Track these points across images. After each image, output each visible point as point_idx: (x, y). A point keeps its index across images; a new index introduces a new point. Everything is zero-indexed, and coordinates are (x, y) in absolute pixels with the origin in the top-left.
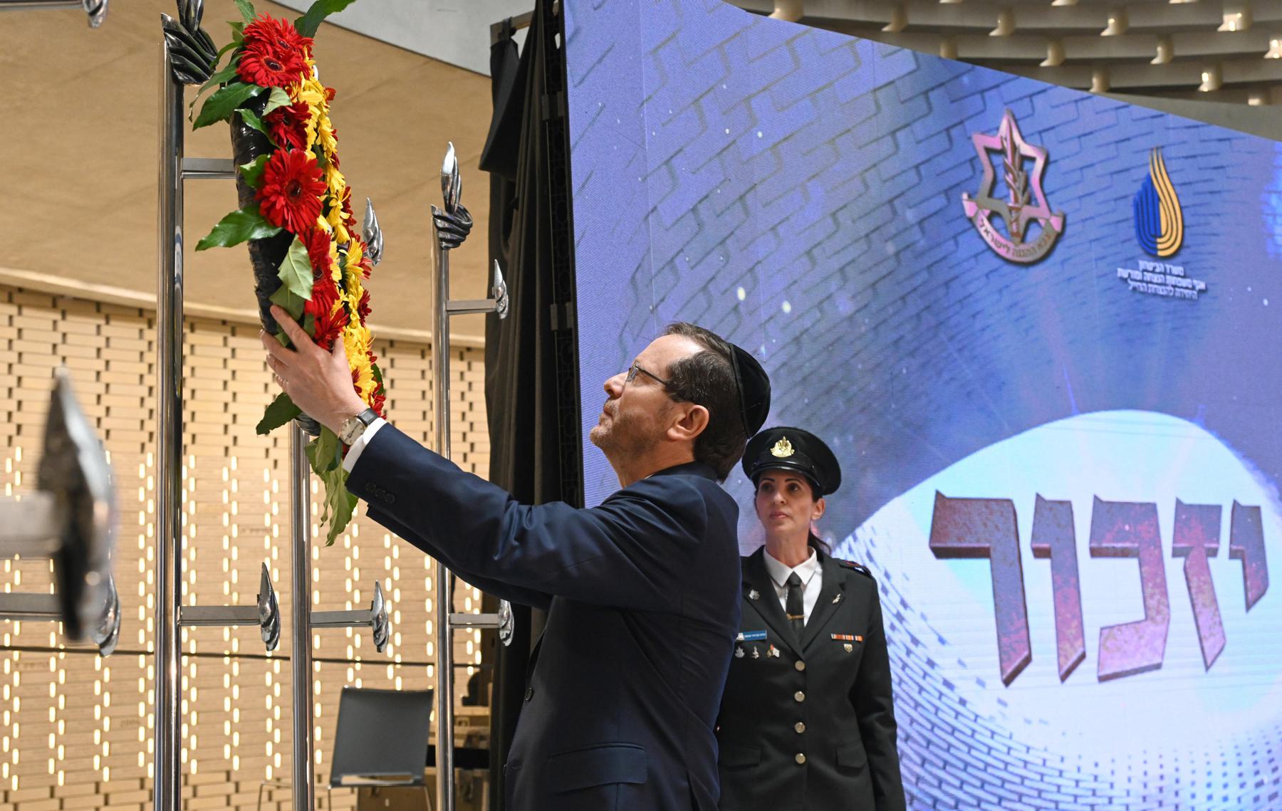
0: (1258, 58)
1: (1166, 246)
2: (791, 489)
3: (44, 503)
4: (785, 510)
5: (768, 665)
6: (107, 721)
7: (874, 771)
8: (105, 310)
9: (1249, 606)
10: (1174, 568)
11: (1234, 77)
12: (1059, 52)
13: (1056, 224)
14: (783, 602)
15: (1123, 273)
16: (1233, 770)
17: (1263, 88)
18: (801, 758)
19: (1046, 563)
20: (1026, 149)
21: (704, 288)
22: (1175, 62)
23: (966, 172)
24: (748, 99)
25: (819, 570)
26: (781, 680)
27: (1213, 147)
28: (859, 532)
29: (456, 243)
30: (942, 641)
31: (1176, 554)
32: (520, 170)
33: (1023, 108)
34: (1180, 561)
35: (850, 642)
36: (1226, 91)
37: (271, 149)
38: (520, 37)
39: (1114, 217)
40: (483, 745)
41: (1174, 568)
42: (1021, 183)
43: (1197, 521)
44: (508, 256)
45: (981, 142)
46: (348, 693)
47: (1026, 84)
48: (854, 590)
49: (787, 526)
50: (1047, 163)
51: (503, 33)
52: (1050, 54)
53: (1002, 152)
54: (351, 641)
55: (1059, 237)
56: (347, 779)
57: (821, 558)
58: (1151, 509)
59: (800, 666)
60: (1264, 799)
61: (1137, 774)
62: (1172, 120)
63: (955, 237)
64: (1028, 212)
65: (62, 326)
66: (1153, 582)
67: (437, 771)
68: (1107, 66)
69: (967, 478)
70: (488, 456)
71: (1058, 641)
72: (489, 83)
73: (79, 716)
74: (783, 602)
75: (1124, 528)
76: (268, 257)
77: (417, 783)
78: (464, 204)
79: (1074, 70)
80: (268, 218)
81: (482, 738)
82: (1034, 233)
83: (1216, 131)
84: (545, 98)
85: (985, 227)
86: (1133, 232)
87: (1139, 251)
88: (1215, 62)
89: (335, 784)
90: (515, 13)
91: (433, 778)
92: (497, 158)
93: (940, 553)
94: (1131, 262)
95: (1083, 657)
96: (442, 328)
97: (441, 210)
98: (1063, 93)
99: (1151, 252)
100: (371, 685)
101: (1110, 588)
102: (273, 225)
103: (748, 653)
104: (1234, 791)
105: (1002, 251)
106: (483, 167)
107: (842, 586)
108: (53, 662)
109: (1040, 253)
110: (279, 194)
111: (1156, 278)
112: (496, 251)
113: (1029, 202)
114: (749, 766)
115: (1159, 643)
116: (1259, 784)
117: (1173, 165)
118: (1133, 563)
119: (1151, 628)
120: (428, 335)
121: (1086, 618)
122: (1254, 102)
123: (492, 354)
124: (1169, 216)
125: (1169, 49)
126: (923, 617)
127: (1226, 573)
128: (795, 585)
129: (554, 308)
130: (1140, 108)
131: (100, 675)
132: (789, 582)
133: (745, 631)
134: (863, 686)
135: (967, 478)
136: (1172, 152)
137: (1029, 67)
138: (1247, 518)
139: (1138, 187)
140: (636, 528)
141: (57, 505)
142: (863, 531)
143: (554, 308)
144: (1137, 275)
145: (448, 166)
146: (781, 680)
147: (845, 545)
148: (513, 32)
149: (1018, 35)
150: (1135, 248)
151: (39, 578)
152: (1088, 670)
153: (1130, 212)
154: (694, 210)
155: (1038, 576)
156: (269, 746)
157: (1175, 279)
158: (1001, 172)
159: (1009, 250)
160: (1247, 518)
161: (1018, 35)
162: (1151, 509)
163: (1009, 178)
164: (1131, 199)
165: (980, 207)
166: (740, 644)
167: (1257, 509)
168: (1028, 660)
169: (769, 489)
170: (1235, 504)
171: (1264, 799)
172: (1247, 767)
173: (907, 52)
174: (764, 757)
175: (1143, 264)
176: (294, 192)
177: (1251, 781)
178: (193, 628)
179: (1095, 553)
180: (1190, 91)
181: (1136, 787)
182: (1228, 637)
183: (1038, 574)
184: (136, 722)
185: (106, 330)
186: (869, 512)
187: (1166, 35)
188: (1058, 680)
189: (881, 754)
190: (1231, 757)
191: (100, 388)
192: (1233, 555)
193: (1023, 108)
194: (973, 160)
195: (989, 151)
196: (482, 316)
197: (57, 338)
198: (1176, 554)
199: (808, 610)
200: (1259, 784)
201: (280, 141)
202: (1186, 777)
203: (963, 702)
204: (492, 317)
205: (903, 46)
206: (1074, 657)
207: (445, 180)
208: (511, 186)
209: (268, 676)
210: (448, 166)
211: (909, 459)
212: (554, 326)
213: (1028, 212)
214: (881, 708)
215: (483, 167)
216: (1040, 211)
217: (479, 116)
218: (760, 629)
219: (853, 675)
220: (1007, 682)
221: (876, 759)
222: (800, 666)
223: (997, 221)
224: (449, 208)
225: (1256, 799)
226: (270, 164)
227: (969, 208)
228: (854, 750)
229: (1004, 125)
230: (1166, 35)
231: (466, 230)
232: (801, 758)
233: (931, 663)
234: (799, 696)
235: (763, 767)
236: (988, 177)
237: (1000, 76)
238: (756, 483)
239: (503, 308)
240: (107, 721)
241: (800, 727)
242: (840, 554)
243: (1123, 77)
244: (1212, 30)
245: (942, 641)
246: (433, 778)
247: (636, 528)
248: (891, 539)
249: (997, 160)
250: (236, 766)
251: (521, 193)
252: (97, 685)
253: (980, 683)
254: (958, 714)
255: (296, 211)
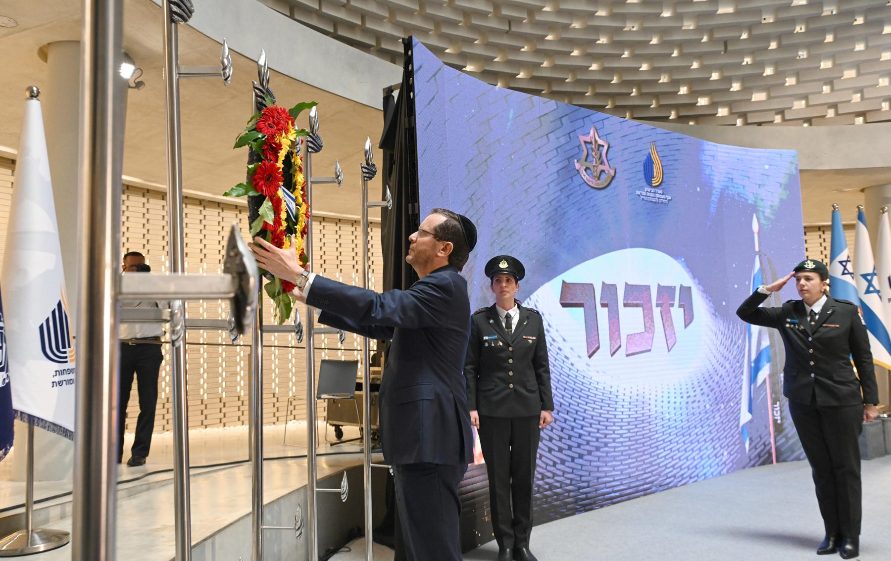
0: (693, 105)
1: (656, 182)
2: (508, 280)
3: (228, 277)
4: (506, 289)
5: (500, 349)
6: (224, 374)
7: (540, 391)
8: (203, 203)
9: (686, 327)
10: (657, 311)
11: (684, 113)
12: (613, 103)
13: (612, 173)
14: (504, 325)
15: (638, 192)
16: (678, 391)
17: (696, 118)
18: (511, 386)
19: (606, 309)
20: (600, 142)
21: (471, 199)
22: (660, 106)
23: (577, 150)
24: (489, 120)
25: (518, 311)
26: (503, 355)
27: (676, 141)
28: (532, 296)
29: (371, 178)
30: (564, 340)
31: (657, 306)
32: (396, 150)
33: (599, 125)
34: (659, 309)
35: (531, 339)
36: (681, 119)
37: (260, 160)
38: (396, 94)
39: (636, 170)
40: (379, 382)
41: (657, 311)
42: (598, 156)
43: (666, 292)
44: (391, 184)
45: (582, 139)
46: (323, 361)
47: (601, 115)
48: (532, 318)
49: (508, 296)
50: (609, 147)
51: (388, 92)
52: (610, 103)
53: (591, 143)
54: (323, 341)
55: (613, 177)
56: (323, 396)
57: (519, 307)
58: (648, 288)
59: (511, 349)
60: (690, 403)
61: (628, 394)
62: (659, 130)
63: (571, 178)
64: (601, 167)
65: (204, 212)
66: (648, 316)
67: (363, 393)
68: (632, 108)
69: (576, 275)
70: (382, 267)
71: (610, 340)
72: (382, 113)
73: (212, 371)
74: (504, 325)
75: (637, 295)
76: (256, 203)
77: (352, 397)
78: (373, 162)
79: (619, 109)
80: (256, 187)
81: (378, 379)
82: (603, 176)
83: (677, 135)
84: (407, 119)
85: (583, 173)
86: (643, 176)
87: (645, 184)
88: (676, 107)
89: (319, 398)
90: (393, 84)
91: (362, 396)
92: (387, 143)
93: (564, 305)
94: (641, 188)
95: (620, 346)
96: (365, 214)
97: (364, 164)
98: (615, 119)
99: (650, 184)
100: (331, 358)
101: (631, 319)
102: (257, 191)
103: (490, 344)
104: (678, 400)
105: (590, 184)
106: (380, 147)
107: (528, 318)
108: (202, 350)
109: (606, 184)
110: (262, 179)
111: (652, 195)
112: (385, 182)
113: (601, 164)
114: (490, 390)
115: (650, 341)
116: (688, 397)
117: (659, 149)
118: (640, 309)
119: (648, 335)
120: (358, 217)
121: (621, 331)
122: (691, 123)
123: (384, 225)
124: (657, 170)
125: (658, 101)
126: (557, 331)
127: (677, 313)
128: (508, 317)
129: (410, 205)
130: (647, 125)
131: (221, 355)
132: (506, 316)
133: (488, 336)
134: (537, 358)
135: (576, 275)
136: (659, 143)
137: (601, 108)
138: (686, 291)
139: (644, 158)
140: (425, 296)
141: (233, 278)
142: (534, 296)
143: (410, 205)
144: (644, 193)
145: (367, 147)
146: (503, 355)
147: (526, 302)
148: (392, 91)
149: (597, 95)
150: (643, 182)
151: (223, 311)
152: (622, 352)
153: (642, 168)
154: (467, 165)
155: (603, 314)
156: (290, 384)
157: (659, 195)
158: (590, 151)
159: (594, 183)
160: (686, 291)
161: (597, 95)
162: (648, 288)
163: (594, 154)
164: (642, 163)
165: (582, 165)
166: (486, 341)
167: (690, 288)
168: (598, 348)
169: (499, 281)
170: (681, 286)
171: (690, 403)
172: (684, 391)
173: (553, 101)
174: (496, 386)
175: (646, 189)
176: (268, 179)
177: (685, 396)
178: (276, 334)
179: (625, 305)
180: (665, 119)
181: (627, 399)
182: (678, 339)
183: (603, 314)
184: (236, 374)
185: (222, 214)
186: (536, 289)
187: (656, 96)
188: (609, 354)
189: (544, 385)
190: (678, 387)
191: (202, 246)
192: (680, 306)
193: (599, 125)
194: (579, 146)
195: (586, 142)
196: (380, 209)
197: (202, 217)
198: (657, 306)
199: (514, 327)
200: (688, 397)
201: (266, 157)
202: (647, 392)
203: (572, 365)
204: (385, 210)
205: (551, 99)
206: (617, 347)
207: (366, 152)
208: (392, 156)
209: (290, 356)
210: (367, 146)
211: (550, 270)
212: (410, 212)
213: (601, 167)
214: (543, 366)
215: (380, 147)
216: (605, 167)
217: (378, 127)
218: (494, 335)
219: (533, 354)
220: (590, 357)
221: (542, 387)
222: (511, 349)
223: (588, 171)
224: (368, 164)
225: (687, 403)
226: (260, 167)
227: (577, 166)
228: (532, 382)
229: (592, 132)
230: (656, 96)
231: (375, 172)
232: (511, 386)
233: (560, 349)
234: (511, 361)
235: (496, 390)
236: (585, 153)
237: (591, 111)
238: (492, 279)
239: (390, 204)
240: (224, 374)
241: (511, 373)
242: (524, 305)
243: (639, 113)
244: (675, 93)
245: (564, 340)
246: (362, 396)
247: (425, 296)
248: (545, 299)
249: (589, 146)
250: (277, 391)
251: (396, 158)
252: (220, 359)
253: (579, 357)
254: (570, 369)
255: (268, 187)
